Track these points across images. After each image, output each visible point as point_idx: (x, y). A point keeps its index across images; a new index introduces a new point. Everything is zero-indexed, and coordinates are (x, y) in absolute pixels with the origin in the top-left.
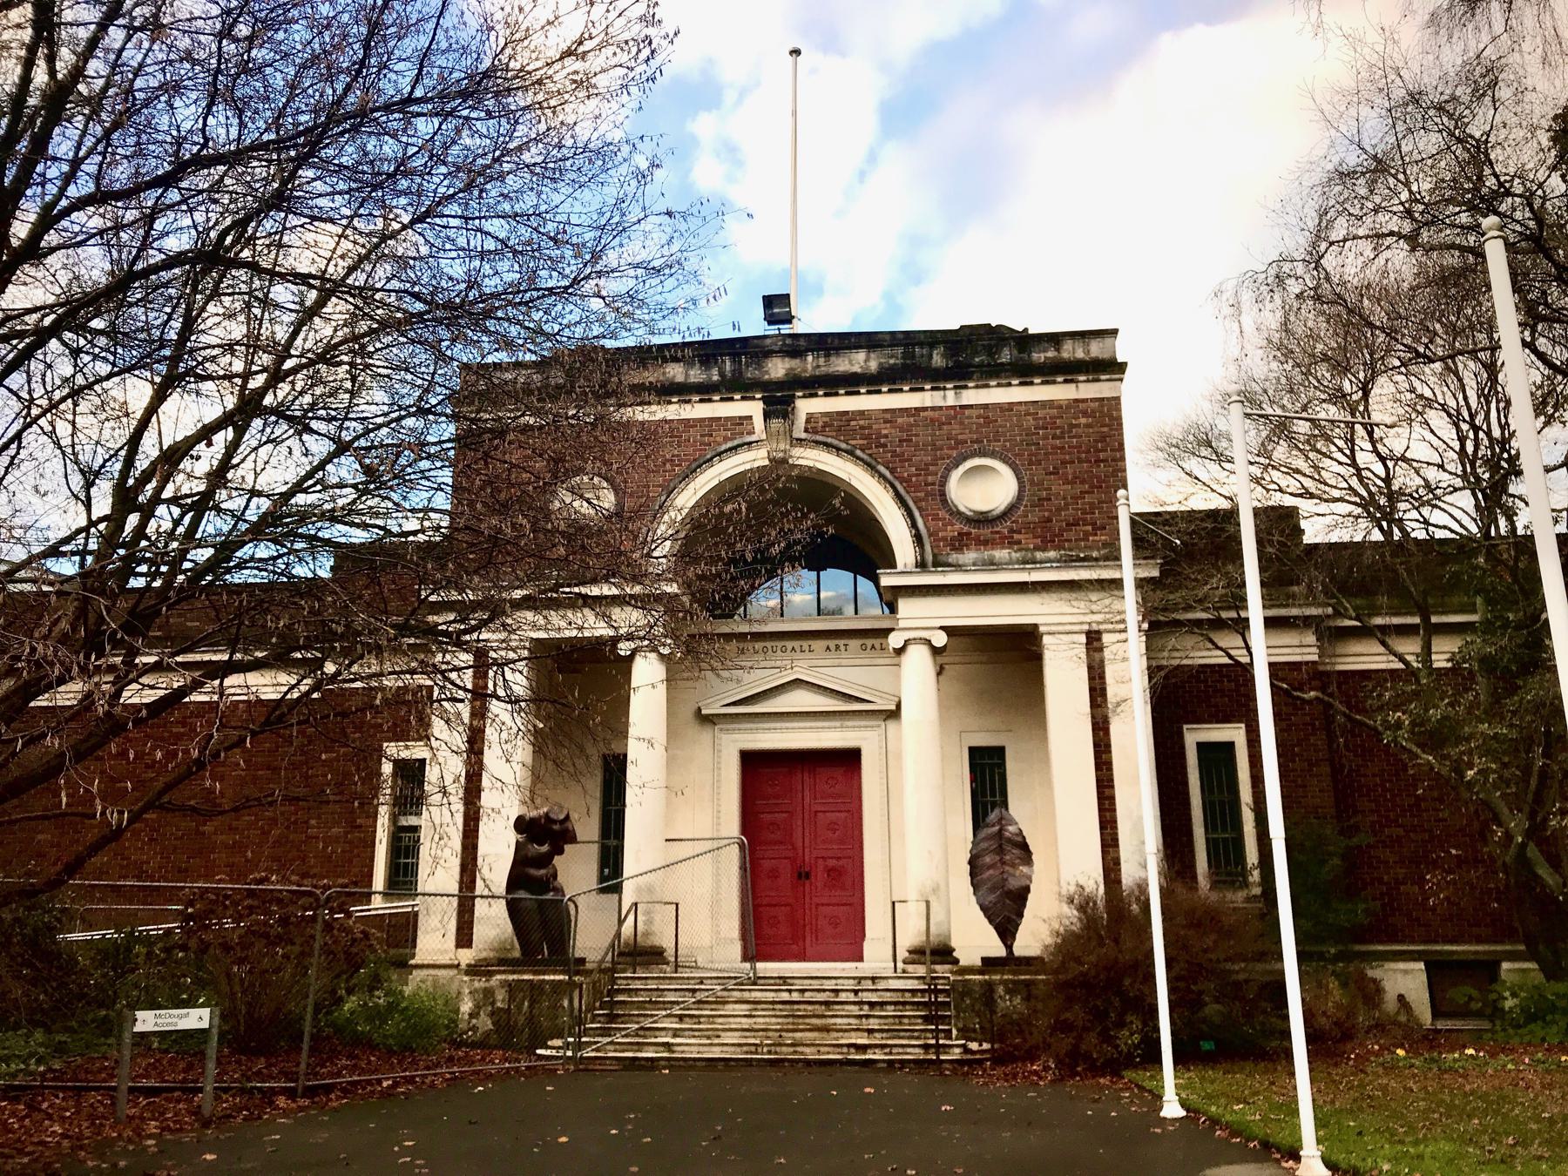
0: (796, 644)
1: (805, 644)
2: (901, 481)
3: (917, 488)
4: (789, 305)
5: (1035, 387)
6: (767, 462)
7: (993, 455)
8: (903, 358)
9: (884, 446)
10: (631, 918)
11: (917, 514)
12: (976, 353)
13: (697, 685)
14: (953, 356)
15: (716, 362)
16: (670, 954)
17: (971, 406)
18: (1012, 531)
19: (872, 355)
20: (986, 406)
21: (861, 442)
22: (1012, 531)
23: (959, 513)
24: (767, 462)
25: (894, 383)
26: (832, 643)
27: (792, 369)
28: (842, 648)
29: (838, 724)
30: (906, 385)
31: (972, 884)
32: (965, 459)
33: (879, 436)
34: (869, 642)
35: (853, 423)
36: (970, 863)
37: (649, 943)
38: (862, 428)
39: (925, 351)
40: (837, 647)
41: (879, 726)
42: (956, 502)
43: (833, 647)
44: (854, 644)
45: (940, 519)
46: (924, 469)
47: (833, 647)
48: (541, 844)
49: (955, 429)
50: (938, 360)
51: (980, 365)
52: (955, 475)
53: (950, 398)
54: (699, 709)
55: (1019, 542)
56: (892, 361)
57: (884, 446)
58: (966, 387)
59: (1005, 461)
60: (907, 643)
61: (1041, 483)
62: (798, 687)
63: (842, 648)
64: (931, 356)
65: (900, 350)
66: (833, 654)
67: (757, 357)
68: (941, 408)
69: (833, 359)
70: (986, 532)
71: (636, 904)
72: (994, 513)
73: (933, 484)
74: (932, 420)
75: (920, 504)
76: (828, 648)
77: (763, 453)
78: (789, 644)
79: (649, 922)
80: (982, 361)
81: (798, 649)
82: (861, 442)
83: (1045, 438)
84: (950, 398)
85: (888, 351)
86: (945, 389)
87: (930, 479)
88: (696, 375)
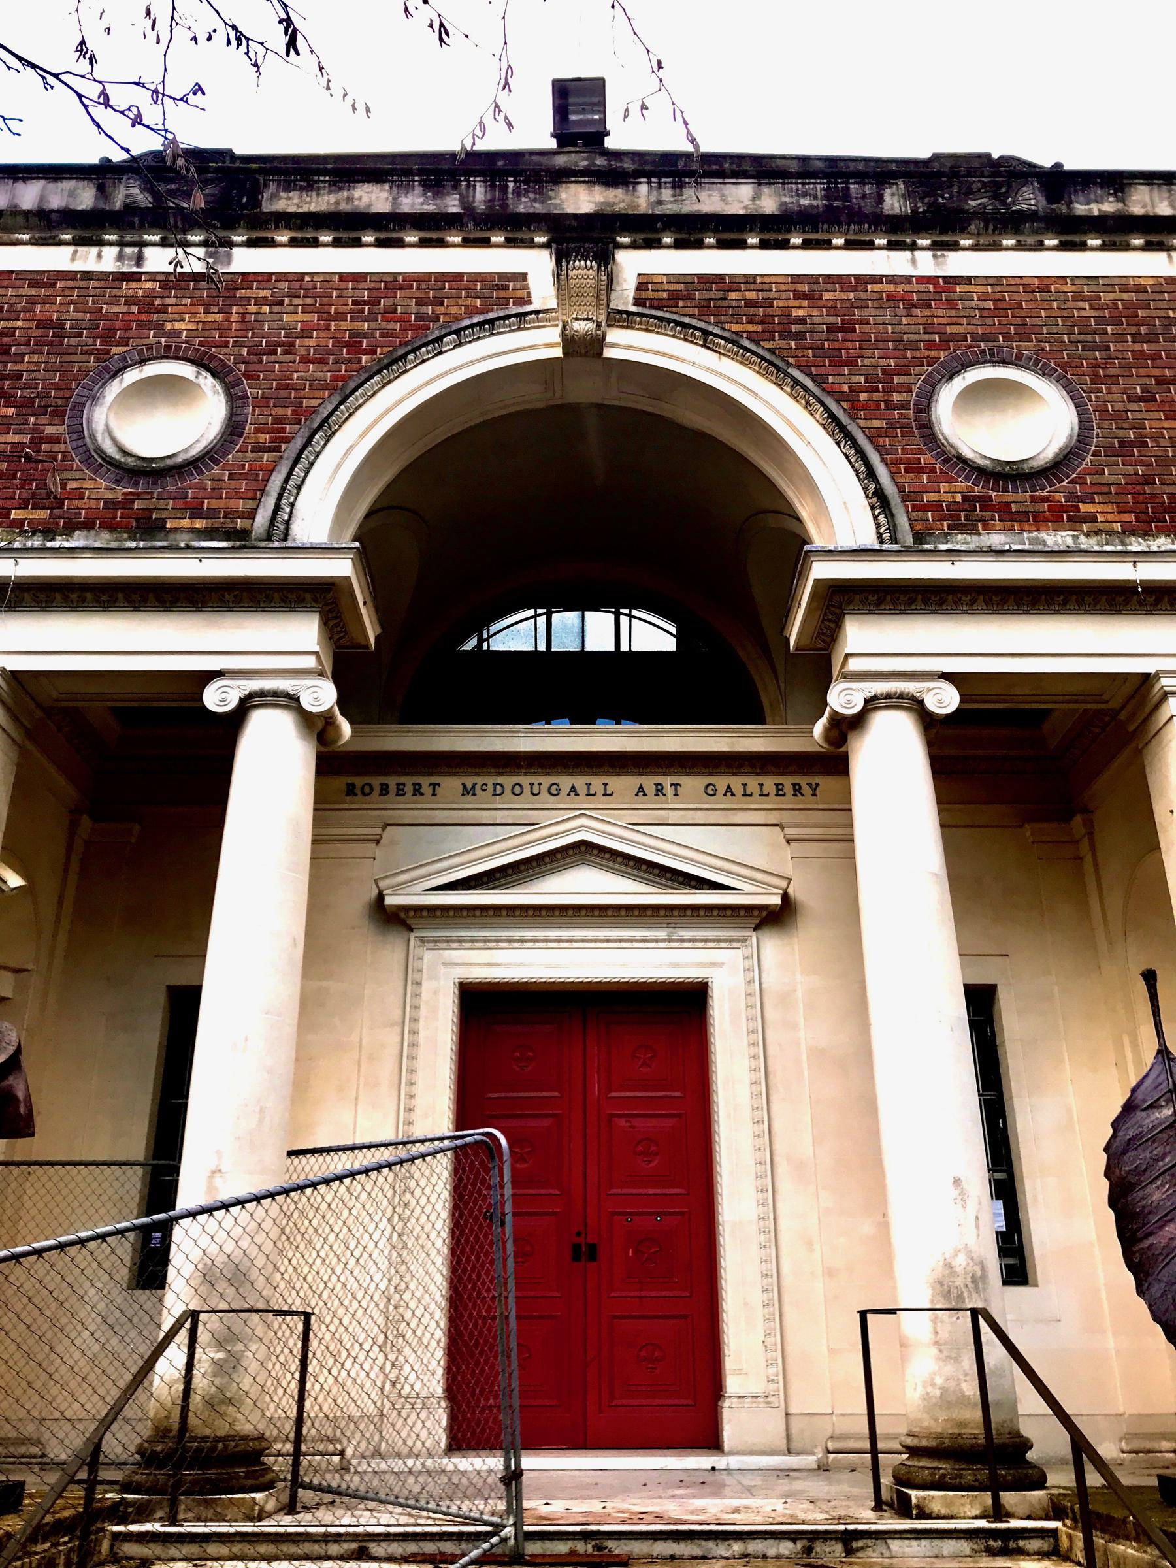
0: (580, 781)
1: (597, 782)
2: (839, 398)
3: (872, 409)
4: (601, 106)
5: (1088, 254)
6: (558, 352)
7: (1016, 362)
8: (826, 197)
9: (799, 336)
10: (175, 1355)
11: (874, 458)
12: (970, 193)
13: (378, 852)
14: (927, 195)
15: (456, 187)
16: (280, 1465)
17: (967, 280)
18: (1071, 496)
19: (766, 190)
20: (997, 281)
21: (751, 327)
22: (1071, 496)
23: (961, 459)
24: (558, 352)
25: (816, 230)
26: (649, 782)
27: (607, 204)
28: (669, 791)
29: (662, 933)
30: (840, 234)
31: (1131, 1265)
32: (965, 366)
33: (787, 317)
34: (721, 782)
35: (733, 295)
36: (1112, 1203)
37: (222, 1430)
38: (751, 304)
39: (868, 189)
40: (659, 789)
41: (744, 940)
42: (954, 440)
43: (650, 789)
44: (692, 784)
45: (922, 470)
46: (883, 381)
47: (650, 789)
48: (995, 1540)
49: (942, 316)
50: (894, 202)
51: (980, 214)
52: (947, 396)
53: (925, 263)
54: (381, 897)
55: (1092, 519)
56: (805, 202)
57: (799, 336)
58: (955, 247)
59: (1045, 373)
60: (872, 704)
61: (1120, 416)
62: (584, 863)
63: (669, 791)
64: (880, 199)
65: (820, 187)
66: (651, 801)
67: (539, 181)
68: (908, 279)
69: (689, 192)
70: (1018, 498)
71: (194, 1315)
72: (1036, 464)
73: (904, 406)
74: (891, 298)
75: (880, 441)
76: (641, 790)
77: (553, 334)
78: (566, 781)
79: (228, 1367)
80: (983, 205)
81: (582, 790)
82: (751, 327)
83: (1120, 338)
84: (925, 263)
85: (796, 185)
86: (913, 247)
87: (896, 397)
88: (414, 202)
